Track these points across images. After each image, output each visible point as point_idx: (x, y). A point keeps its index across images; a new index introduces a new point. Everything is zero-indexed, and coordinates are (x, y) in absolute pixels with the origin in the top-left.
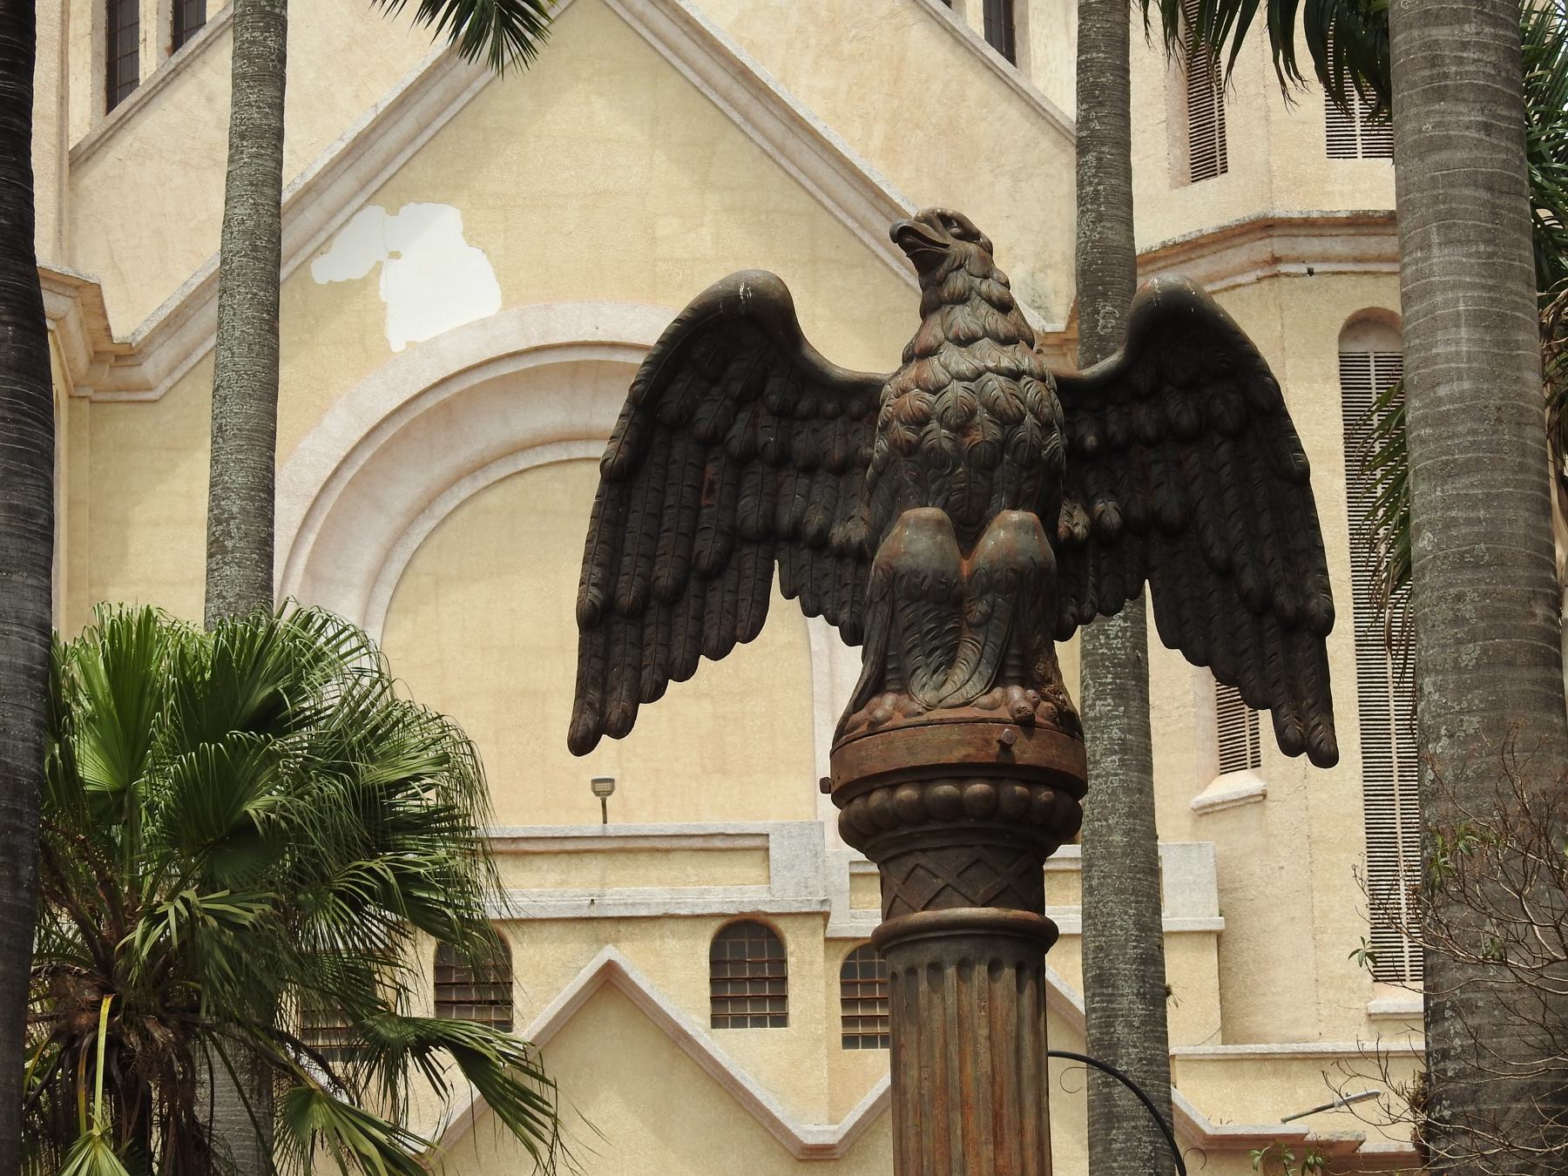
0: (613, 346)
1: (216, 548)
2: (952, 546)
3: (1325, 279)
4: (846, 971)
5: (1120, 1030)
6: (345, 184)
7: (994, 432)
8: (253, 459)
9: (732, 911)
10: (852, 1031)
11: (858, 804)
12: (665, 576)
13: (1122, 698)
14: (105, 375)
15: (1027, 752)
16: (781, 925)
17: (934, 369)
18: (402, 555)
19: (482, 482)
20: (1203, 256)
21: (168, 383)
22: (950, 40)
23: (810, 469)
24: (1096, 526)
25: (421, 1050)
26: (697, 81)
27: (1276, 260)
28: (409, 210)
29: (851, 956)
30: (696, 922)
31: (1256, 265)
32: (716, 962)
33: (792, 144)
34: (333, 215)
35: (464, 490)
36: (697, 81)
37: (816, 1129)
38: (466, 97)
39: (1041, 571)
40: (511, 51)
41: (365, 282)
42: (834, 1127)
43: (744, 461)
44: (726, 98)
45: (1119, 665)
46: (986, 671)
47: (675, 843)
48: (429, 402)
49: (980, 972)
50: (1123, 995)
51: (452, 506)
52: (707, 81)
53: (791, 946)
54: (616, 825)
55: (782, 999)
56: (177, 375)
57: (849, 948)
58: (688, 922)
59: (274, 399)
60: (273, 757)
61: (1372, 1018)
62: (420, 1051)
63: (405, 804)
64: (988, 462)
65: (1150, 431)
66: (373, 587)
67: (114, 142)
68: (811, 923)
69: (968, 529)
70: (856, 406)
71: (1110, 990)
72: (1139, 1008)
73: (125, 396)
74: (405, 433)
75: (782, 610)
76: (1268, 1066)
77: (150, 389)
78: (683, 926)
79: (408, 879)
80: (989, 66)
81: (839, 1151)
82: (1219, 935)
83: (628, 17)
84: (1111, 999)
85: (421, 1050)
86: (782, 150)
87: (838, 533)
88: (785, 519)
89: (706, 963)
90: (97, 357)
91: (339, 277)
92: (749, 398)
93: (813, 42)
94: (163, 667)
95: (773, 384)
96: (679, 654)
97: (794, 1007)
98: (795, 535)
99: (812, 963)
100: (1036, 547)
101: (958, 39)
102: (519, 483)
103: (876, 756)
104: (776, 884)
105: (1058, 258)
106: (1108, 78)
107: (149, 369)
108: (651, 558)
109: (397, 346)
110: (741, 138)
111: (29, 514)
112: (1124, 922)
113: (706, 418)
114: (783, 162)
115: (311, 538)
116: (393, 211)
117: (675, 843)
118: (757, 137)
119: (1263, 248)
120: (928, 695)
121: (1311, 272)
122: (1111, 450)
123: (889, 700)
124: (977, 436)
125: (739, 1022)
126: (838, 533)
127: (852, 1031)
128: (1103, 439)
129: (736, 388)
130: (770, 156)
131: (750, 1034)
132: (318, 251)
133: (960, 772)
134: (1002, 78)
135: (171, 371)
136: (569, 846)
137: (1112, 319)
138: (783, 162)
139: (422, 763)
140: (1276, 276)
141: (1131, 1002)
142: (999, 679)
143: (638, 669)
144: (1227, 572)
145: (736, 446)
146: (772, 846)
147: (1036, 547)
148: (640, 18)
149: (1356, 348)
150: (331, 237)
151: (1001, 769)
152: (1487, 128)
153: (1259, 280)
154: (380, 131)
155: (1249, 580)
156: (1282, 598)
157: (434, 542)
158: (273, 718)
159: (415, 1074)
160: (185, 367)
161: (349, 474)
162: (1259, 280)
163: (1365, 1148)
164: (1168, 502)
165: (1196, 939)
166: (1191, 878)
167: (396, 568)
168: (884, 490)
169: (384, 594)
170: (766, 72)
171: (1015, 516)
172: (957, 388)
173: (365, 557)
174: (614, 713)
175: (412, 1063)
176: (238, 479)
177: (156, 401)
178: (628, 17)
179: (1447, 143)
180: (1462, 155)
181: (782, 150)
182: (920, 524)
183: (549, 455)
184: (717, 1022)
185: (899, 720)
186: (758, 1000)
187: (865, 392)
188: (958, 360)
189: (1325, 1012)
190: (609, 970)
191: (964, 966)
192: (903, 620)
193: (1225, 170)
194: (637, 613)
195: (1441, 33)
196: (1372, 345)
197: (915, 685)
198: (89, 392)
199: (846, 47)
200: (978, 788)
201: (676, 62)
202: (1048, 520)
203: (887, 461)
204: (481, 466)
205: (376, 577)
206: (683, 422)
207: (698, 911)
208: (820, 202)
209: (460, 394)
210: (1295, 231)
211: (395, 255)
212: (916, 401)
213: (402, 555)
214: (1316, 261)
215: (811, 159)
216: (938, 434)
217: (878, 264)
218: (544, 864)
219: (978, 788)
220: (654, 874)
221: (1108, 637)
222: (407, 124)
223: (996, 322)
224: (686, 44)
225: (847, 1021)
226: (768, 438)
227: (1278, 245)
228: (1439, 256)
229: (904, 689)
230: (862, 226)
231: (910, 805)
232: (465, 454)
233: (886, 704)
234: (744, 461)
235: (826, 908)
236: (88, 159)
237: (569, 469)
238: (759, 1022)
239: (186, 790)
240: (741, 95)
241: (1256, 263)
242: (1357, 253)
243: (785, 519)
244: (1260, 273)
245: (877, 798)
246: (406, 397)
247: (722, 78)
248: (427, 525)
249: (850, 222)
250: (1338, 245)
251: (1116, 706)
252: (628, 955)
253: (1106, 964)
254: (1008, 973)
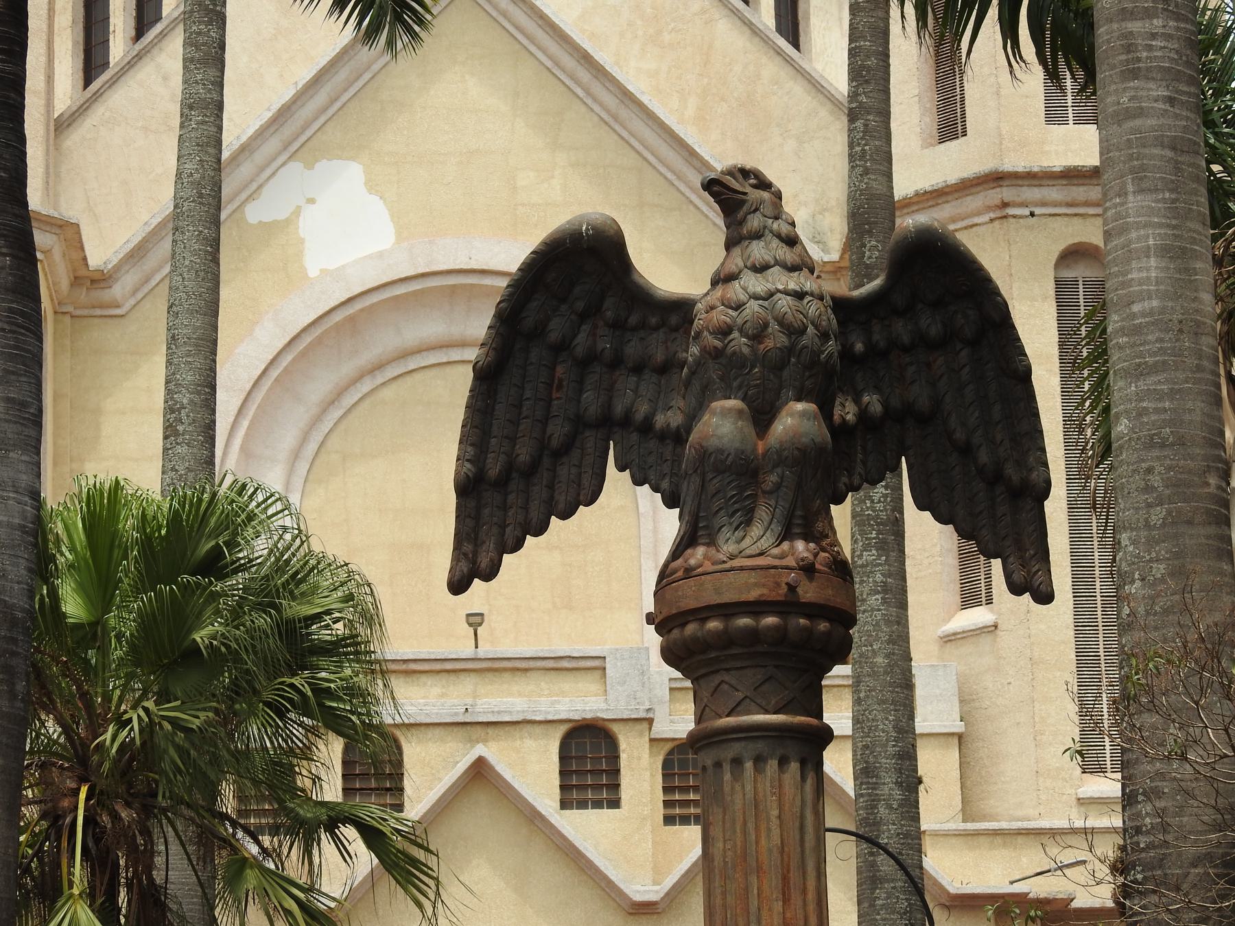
0: (483, 272)
1: (170, 431)
2: (750, 430)
3: (1044, 220)
4: (667, 764)
5: (882, 811)
6: (272, 145)
7: (783, 340)
8: (199, 362)
9: (577, 718)
10: (671, 812)
11: (676, 633)
12: (524, 454)
13: (884, 549)
14: (82, 295)
15: (809, 592)
16: (615, 728)
17: (735, 291)
18: (317, 437)
19: (380, 380)
20: (947, 202)
21: (132, 302)
22: (748, 32)
23: (638, 369)
24: (863, 414)
25: (331, 827)
26: (549, 64)
27: (1005, 205)
28: (322, 165)
29: (671, 753)
30: (549, 726)
31: (989, 209)
32: (564, 758)
33: (624, 113)
34: (262, 169)
35: (366, 386)
36: (549, 64)
37: (643, 889)
38: (367, 76)
39: (820, 449)
40: (402, 40)
41: (288, 222)
42: (657, 888)
43: (586, 363)
44: (572, 77)
45: (881, 524)
46: (777, 528)
47: (532, 664)
48: (338, 317)
49: (772, 765)
50: (884, 784)
51: (356, 399)
52: (557, 64)
53: (623, 745)
54: (485, 650)
55: (616, 787)
56: (140, 295)
57: (669, 746)
58: (542, 726)
59: (216, 314)
60: (215, 596)
61: (1081, 802)
62: (331, 828)
63: (319, 633)
64: (778, 363)
65: (906, 339)
66: (294, 462)
67: (90, 112)
68: (639, 727)
69: (762, 416)
70: (674, 320)
71: (874, 780)
72: (897, 794)
73: (98, 312)
74: (319, 341)
75: (616, 481)
76: (999, 840)
77: (118, 306)
78: (538, 729)
79: (321, 692)
80: (779, 52)
81: (661, 906)
82: (960, 737)
83: (494, 14)
84: (875, 786)
85: (331, 827)
86: (616, 118)
87: (660, 420)
88: (619, 409)
89: (556, 758)
90: (76, 281)
91: (267, 218)
92: (590, 313)
93: (640, 33)
94: (128, 525)
95: (609, 303)
96: (535, 515)
97: (626, 793)
98: (626, 422)
99: (639, 758)
100: (816, 431)
101: (754, 31)
102: (409, 380)
103: (690, 595)
104: (611, 696)
105: (833, 203)
106: (872, 62)
107: (118, 290)
108: (513, 440)
109: (313, 272)
110: (583, 109)
111: (23, 405)
112: (885, 726)
113: (556, 329)
114: (617, 127)
115: (245, 423)
116: (309, 166)
117: (532, 664)
118: (596, 108)
119: (995, 195)
120: (731, 548)
121: (1032, 214)
122: (875, 354)
123: (700, 551)
124: (769, 343)
125: (582, 805)
126: (660, 420)
127: (671, 812)
128: (869, 345)
129: (580, 306)
130: (606, 123)
131: (591, 815)
132: (250, 198)
133: (756, 608)
134: (789, 61)
135: (134, 292)
136: (449, 666)
137: (875, 251)
138: (617, 127)
139: (332, 600)
140: (1005, 217)
141: (891, 789)
142: (786, 535)
143: (503, 527)
144: (966, 451)
145: (579, 351)
146: (608, 666)
147: (816, 431)
148: (504, 14)
149: (1068, 274)
150: (260, 187)
151: (788, 605)
152: (1171, 100)
153: (992, 220)
154: (299, 103)
155: (984, 457)
156: (1010, 471)
157: (342, 427)
158: (215, 565)
159: (327, 846)
160: (146, 289)
161: (275, 373)
162: (992, 220)
163: (1075, 904)
164: (920, 395)
165: (942, 739)
167: (312, 447)
168: (696, 386)
169: (303, 468)
170: (603, 57)
171: (800, 406)
172: (754, 306)
173: (288, 439)
174: (484, 562)
175: (324, 837)
176: (188, 377)
177: (122, 316)
178: (494, 14)
179: (1140, 113)
180: (1152, 122)
181: (616, 118)
182: (725, 413)
183: (432, 358)
184: (565, 804)
185: (708, 567)
186: (597, 787)
187: (681, 308)
188: (755, 283)
189: (1043, 797)
190: (480, 764)
191: (759, 760)
192: (711, 488)
193: (964, 134)
194: (502, 483)
195: (1135, 26)
196: (1080, 272)
197: (721, 539)
198: (70, 309)
199: (667, 37)
200: (770, 620)
201: (533, 48)
202: (826, 409)
203: (699, 363)
204: (379, 367)
205: (296, 455)
206: (538, 332)
207: (550, 717)
208: (645, 159)
209: (362, 310)
210: (1020, 182)
211: (311, 201)
212: (722, 316)
213: (317, 437)
214: (1036, 205)
215: (639, 126)
216: (739, 342)
217: (691, 207)
218: (428, 680)
219: (770, 620)
220: (515, 688)
221: (872, 502)
222: (321, 98)
223: (785, 253)
224: (540, 35)
225: (667, 804)
226: (605, 345)
227: (1007, 193)
228: (1134, 202)
229: (712, 543)
230: (679, 178)
231: (717, 634)
232: (366, 357)
233: (698, 554)
234: (586, 363)
235: (650, 715)
236: (69, 125)
237: (448, 369)
238: (598, 804)
239: (147, 622)
240: (584, 75)
241: (989, 207)
242: (1069, 199)
243: (619, 409)
244: (992, 215)
245: (691, 628)
246: (320, 312)
247: (569, 62)
248: (336, 414)
249: (669, 175)
250: (1053, 193)
251: (879, 556)
252: (495, 752)
253: (871, 759)
254: (794, 766)
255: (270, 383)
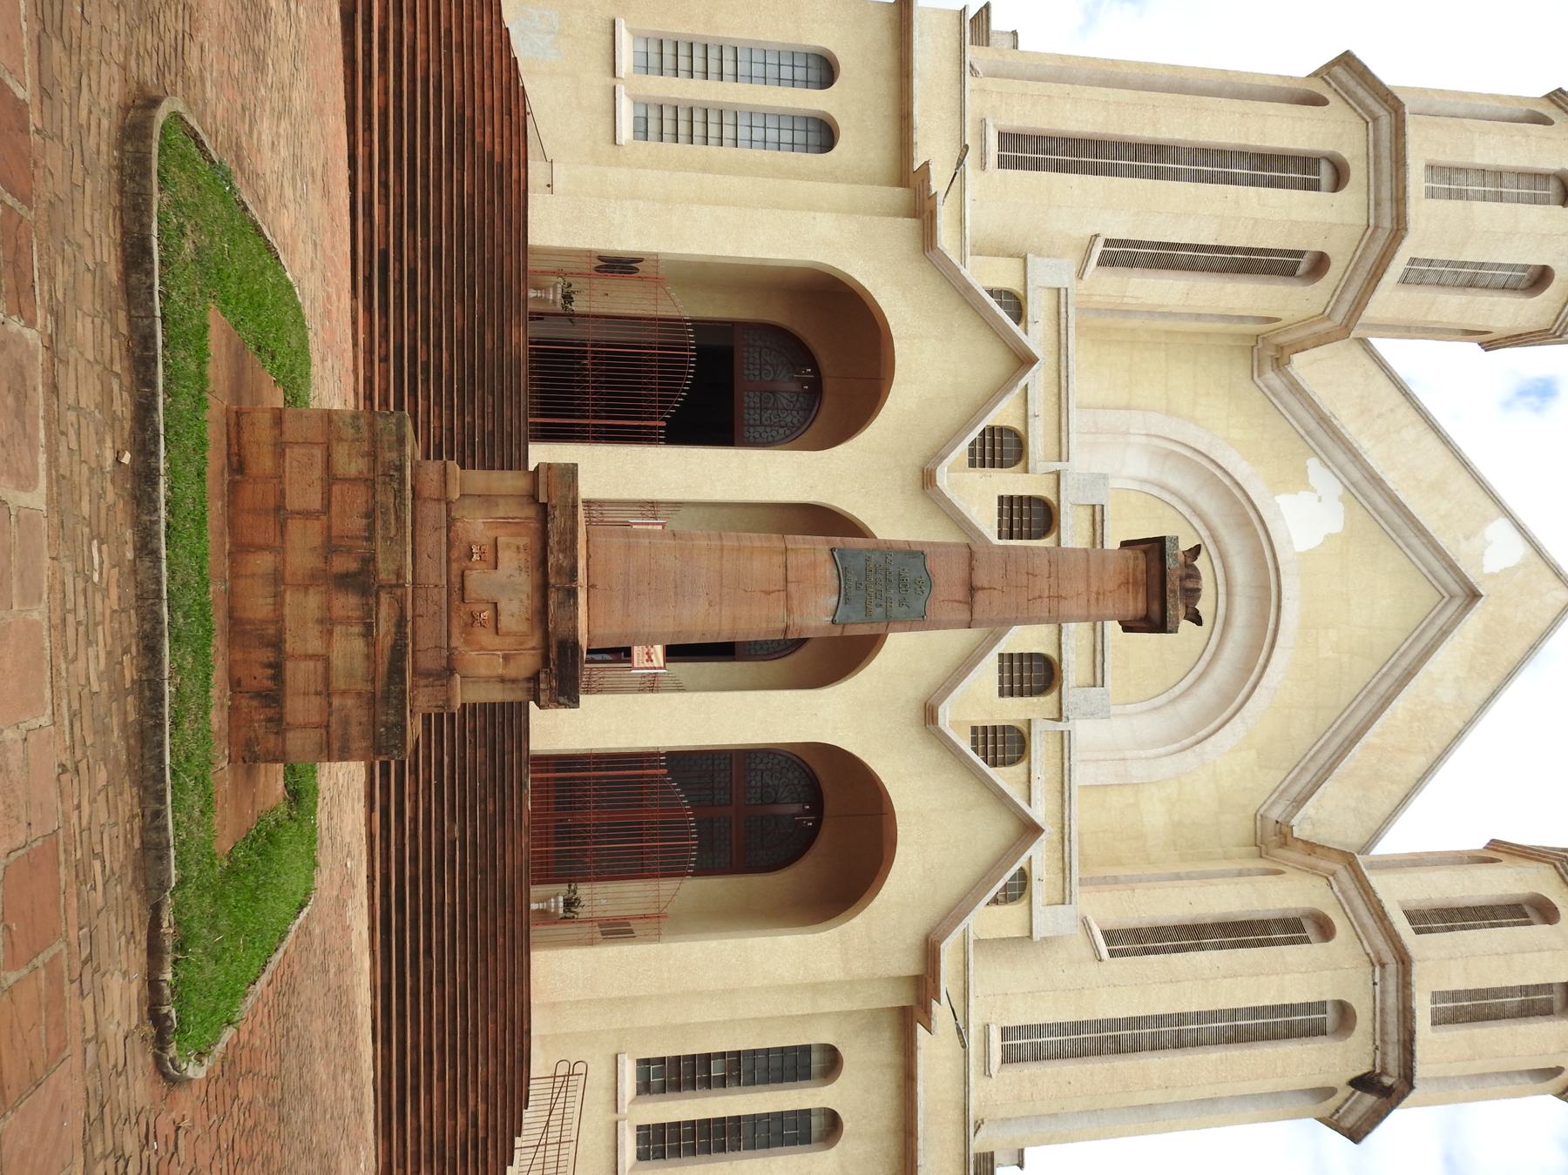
0: (1279, 607)
3: (1371, 992)
6: (1356, 475)
9: (1063, 666)
10: (980, 731)
14: (1271, 352)
16: (1055, 694)
20: (1375, 922)
21: (1261, 385)
22: (1419, 776)
26: (1401, 650)
27: (1383, 966)
28: (1341, 507)
29: (1019, 731)
30: (1056, 645)
32: (1031, 656)
33: (1374, 698)
34: (1341, 470)
36: (1401, 650)
38: (1394, 536)
41: (1308, 484)
42: (947, 724)
44: (1393, 665)
47: (1099, 634)
51: (1196, 526)
52: (1402, 655)
53: (1042, 699)
56: (1265, 390)
58: (1056, 641)
66: (1157, 485)
67: (1372, 362)
73: (1256, 364)
74: (1237, 502)
76: (961, 968)
77: (1259, 376)
81: (931, 727)
82: (1030, 936)
83: (1431, 616)
86: (1370, 692)
89: (1034, 651)
90: (1280, 348)
91: (1310, 472)
93: (1418, 708)
97: (1008, 700)
99: (1033, 711)
104: (1078, 691)
105: (1318, 831)
107: (1271, 377)
109: (1278, 499)
110: (1374, 672)
114: (1364, 693)
115: (1189, 453)
116: (1341, 499)
117: (1099, 634)
118: (1375, 680)
119: (1389, 957)
121: (1375, 984)
127: (980, 731)
130: (1366, 686)
135: (1268, 387)
138: (1364, 693)
140: (1373, 964)
146: (1097, 689)
148: (1432, 622)
149: (1329, 1008)
150: (1328, 467)
153: (1368, 955)
154: (1382, 492)
156: (252, 439)
157: (1180, 518)
160: (1269, 394)
161: (1218, 473)
162: (1368, 955)
163: (920, 1029)
165: (1028, 925)
166: (1060, 921)
169: (1155, 491)
173: (1175, 482)
177: (1252, 378)
178: (1431, 616)
181: (1370, 692)
184: (1001, 655)
189: (989, 999)
196: (1331, 1017)
198: (1260, 345)
199: (1416, 725)
201: (1410, 640)
205: (1163, 487)
207: (1063, 646)
208: (1345, 710)
209: (1256, 530)
210: (1400, 977)
211: (1320, 500)
214: (1381, 987)
217: (1315, 740)
227: (1392, 967)
230: (1334, 732)
235: (1064, 719)
236: (1365, 349)
237: (1213, 585)
238: (1001, 681)
240: (1397, 672)
241: (1379, 953)
242: (1388, 1010)
244: (1372, 955)
246: (1256, 503)
247: (1405, 663)
248: (1187, 513)
249: (1335, 726)
250: (1392, 1001)
255: (459, 686)
